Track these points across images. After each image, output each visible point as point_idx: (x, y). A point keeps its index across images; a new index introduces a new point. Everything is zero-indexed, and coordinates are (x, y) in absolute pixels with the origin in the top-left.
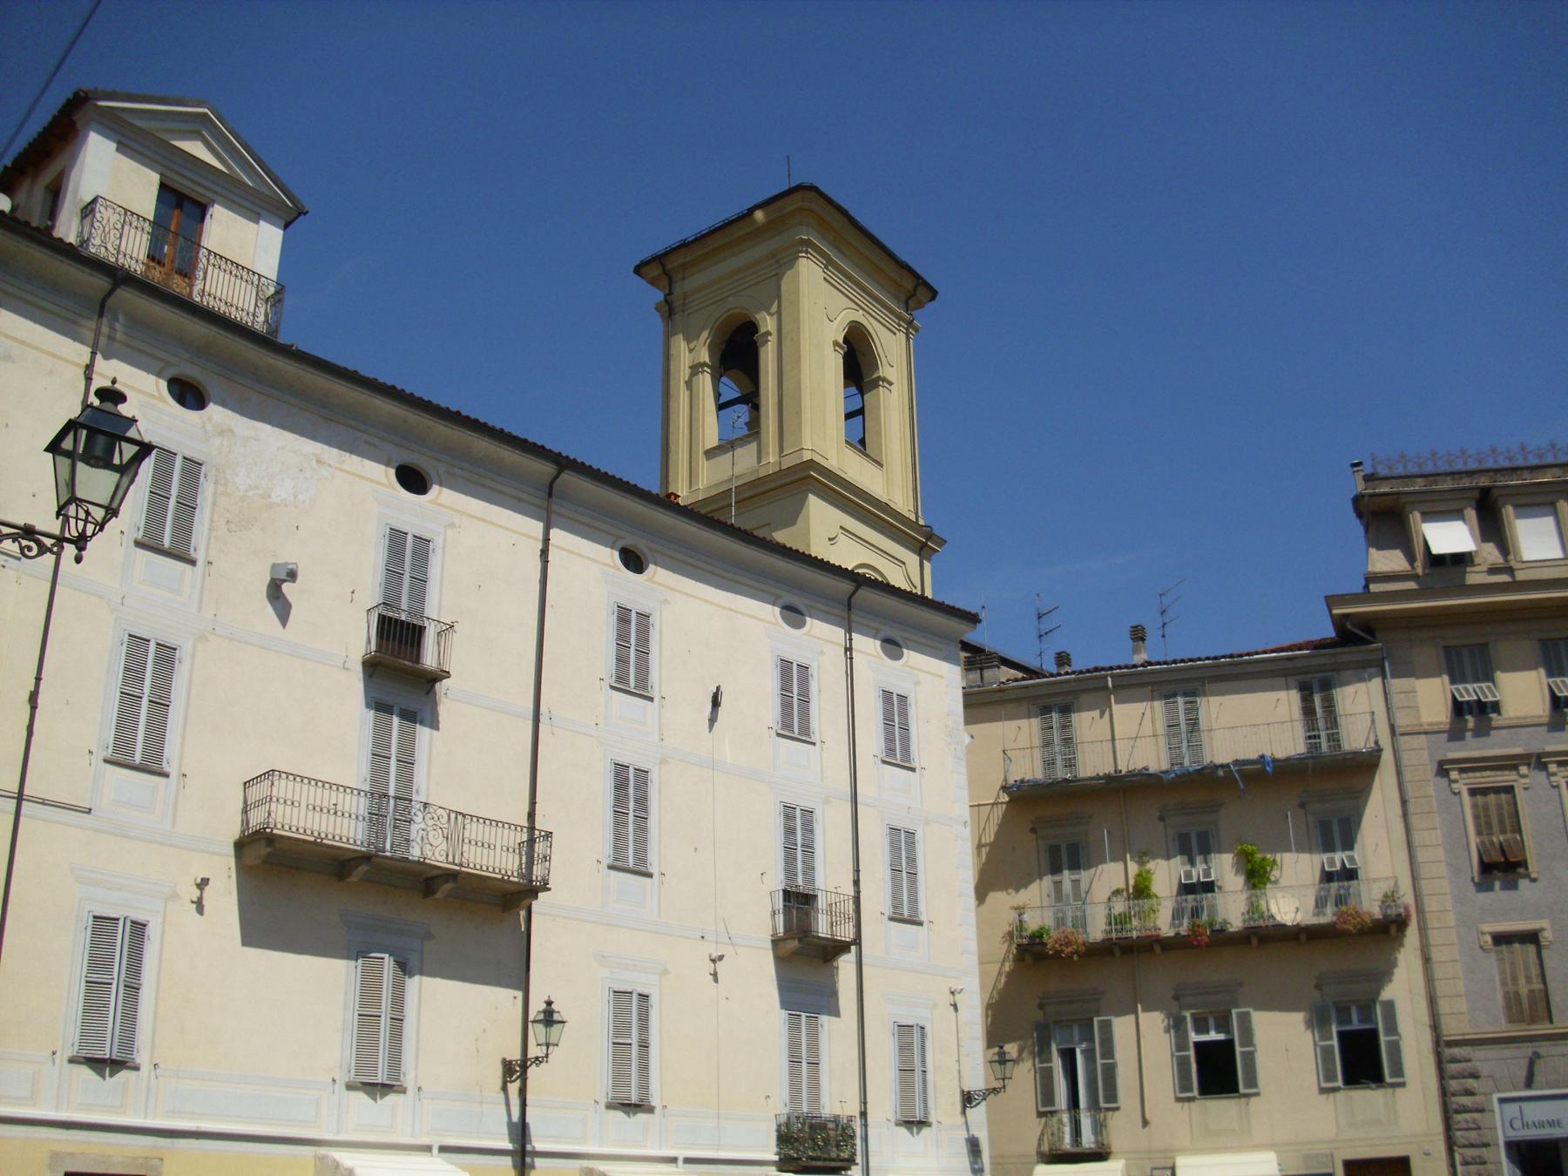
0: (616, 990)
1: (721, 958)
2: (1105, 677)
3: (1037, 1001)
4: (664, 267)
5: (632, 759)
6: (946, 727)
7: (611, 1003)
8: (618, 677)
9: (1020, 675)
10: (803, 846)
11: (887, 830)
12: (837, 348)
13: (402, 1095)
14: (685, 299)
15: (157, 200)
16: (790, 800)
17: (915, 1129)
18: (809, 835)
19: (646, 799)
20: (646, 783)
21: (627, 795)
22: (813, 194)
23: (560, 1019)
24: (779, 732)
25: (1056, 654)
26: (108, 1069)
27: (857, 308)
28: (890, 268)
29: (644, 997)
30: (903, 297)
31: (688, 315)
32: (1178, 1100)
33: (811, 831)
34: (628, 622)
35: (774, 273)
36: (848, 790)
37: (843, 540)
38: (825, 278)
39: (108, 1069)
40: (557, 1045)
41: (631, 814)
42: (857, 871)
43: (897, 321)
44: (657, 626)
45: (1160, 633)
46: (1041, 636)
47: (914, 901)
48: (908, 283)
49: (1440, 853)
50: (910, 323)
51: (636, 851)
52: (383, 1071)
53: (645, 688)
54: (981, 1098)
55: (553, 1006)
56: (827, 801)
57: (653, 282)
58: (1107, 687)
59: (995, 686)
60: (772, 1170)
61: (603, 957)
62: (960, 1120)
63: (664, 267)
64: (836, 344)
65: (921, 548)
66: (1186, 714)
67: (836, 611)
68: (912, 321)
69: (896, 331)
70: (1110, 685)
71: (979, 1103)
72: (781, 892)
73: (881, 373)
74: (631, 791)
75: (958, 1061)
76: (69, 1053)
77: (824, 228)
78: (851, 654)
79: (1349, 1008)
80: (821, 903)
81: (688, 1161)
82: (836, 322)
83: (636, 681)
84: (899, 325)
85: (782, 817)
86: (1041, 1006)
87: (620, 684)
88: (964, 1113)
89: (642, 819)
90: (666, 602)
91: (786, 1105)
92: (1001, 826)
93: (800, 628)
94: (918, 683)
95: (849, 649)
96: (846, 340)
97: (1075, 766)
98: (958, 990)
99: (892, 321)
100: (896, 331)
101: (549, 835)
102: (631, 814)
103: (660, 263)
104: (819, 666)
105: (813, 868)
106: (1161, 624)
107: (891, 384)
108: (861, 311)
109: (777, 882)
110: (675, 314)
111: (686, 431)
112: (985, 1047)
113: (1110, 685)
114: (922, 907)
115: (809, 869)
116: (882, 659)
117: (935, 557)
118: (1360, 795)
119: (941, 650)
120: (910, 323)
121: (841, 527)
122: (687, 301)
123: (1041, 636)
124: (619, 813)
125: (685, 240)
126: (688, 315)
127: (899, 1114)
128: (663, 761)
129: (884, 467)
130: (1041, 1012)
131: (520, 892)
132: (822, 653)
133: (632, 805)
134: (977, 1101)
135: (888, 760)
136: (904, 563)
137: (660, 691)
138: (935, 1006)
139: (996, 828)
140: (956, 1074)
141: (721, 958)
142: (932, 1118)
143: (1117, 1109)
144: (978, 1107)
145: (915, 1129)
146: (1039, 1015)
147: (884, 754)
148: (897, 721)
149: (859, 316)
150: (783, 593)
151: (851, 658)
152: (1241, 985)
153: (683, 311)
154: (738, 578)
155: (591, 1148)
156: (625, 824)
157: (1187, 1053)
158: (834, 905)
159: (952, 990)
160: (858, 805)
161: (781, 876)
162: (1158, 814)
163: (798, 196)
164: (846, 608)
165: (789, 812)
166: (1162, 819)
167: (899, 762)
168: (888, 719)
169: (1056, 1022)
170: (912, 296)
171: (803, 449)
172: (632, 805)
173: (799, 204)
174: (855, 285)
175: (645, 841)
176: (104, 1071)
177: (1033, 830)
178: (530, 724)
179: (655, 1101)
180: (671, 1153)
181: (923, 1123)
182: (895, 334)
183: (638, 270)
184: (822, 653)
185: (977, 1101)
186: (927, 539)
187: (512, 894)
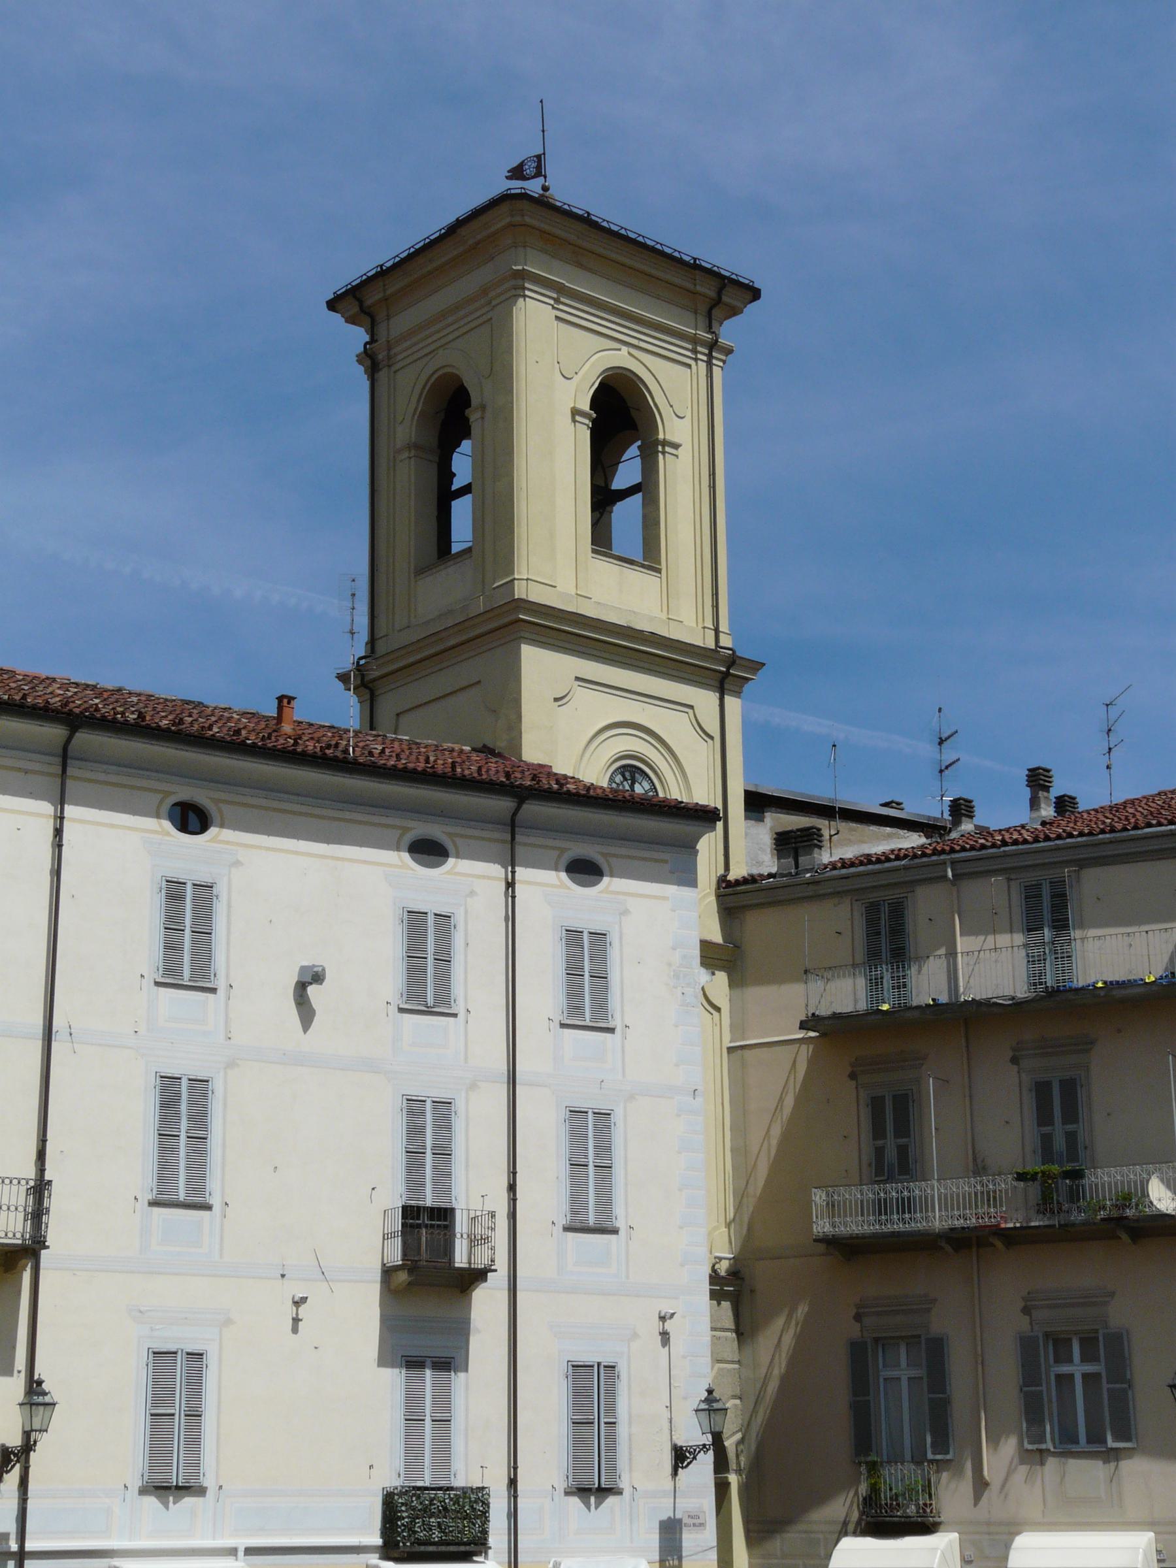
0: (155, 1350)
1: (304, 1300)
2: (944, 863)
4: (361, 302)
5: (185, 1066)
6: (670, 965)
7: (150, 1366)
8: (166, 970)
10: (434, 1147)
11: (564, 1114)
12: (578, 418)
13: (619, 1497)
14: (389, 350)
16: (415, 1091)
17: (593, 1499)
18: (444, 1133)
19: (205, 1115)
20: (205, 1096)
21: (178, 1114)
23: (51, 1401)
24: (401, 1006)
25: (1029, 770)
29: (196, 1356)
30: (703, 309)
31: (395, 372)
33: (449, 1128)
34: (182, 898)
35: (485, 318)
36: (503, 1067)
37: (583, 695)
38: (557, 318)
40: (46, 1431)
41: (183, 1135)
42: (513, 1173)
44: (224, 897)
45: (1104, 761)
46: (941, 771)
47: (605, 1202)
50: (713, 346)
51: (188, 1181)
52: (181, 1390)
53: (206, 977)
54: (692, 1456)
55: (44, 1385)
56: (473, 1086)
57: (351, 320)
58: (946, 876)
59: (808, 875)
60: (374, 1559)
61: (141, 1312)
62: (668, 1484)
63: (361, 302)
64: (575, 412)
66: (1053, 912)
67: (496, 835)
68: (717, 341)
70: (950, 874)
71: (691, 1462)
72: (400, 1209)
74: (184, 1107)
75: (670, 1408)
77: (554, 246)
78: (513, 892)
79: (1070, 1340)
80: (461, 1224)
81: (249, 1551)
82: (577, 379)
83: (193, 970)
85: (405, 1113)
86: (858, 1317)
87: (170, 979)
88: (675, 1473)
89: (199, 1140)
90: (238, 863)
91: (399, 1475)
94: (626, 912)
95: (510, 885)
96: (595, 402)
97: (905, 986)
98: (668, 1316)
99: (682, 350)
101: (50, 1182)
102: (183, 1135)
103: (355, 297)
104: (466, 912)
105: (449, 1175)
106: (1108, 750)
107: (676, 446)
108: (625, 349)
109: (393, 1196)
110: (379, 370)
111: (649, 345)
113: (950, 874)
114: (619, 1209)
115: (443, 1176)
116: (569, 888)
117: (748, 687)
119: (666, 862)
120: (713, 346)
121: (577, 679)
122: (392, 352)
123: (941, 771)
124: (166, 1137)
125: (381, 266)
126: (395, 372)
127: (570, 1479)
128: (231, 1064)
130: (857, 1326)
131: (16, 1251)
132: (472, 893)
133: (184, 1124)
134: (689, 1460)
135: (569, 1022)
136: (691, 707)
137: (227, 976)
138: (635, 1336)
140: (666, 1426)
141: (304, 1300)
142: (624, 1484)
144: (691, 1466)
145: (593, 1499)
146: (855, 1330)
147: (565, 1014)
148: (587, 968)
149: (622, 358)
150: (410, 824)
151: (513, 897)
153: (389, 366)
154: (347, 815)
155: (115, 1543)
156: (174, 1149)
158: (480, 1218)
159: (662, 1314)
160: (518, 1087)
161: (401, 1188)
162: (1011, 1054)
163: (504, 208)
165: (414, 1107)
166: (1015, 1060)
167: (588, 1023)
168: (573, 971)
169: (877, 1340)
170: (717, 302)
171: (515, 579)
172: (184, 1124)
173: (508, 220)
175: (203, 1166)
177: (853, 1076)
178: (38, 1046)
179: (208, 1481)
180: (229, 1542)
181: (604, 1492)
182: (689, 366)
183: (332, 305)
184: (472, 893)
185: (689, 1460)
187: (11, 1252)
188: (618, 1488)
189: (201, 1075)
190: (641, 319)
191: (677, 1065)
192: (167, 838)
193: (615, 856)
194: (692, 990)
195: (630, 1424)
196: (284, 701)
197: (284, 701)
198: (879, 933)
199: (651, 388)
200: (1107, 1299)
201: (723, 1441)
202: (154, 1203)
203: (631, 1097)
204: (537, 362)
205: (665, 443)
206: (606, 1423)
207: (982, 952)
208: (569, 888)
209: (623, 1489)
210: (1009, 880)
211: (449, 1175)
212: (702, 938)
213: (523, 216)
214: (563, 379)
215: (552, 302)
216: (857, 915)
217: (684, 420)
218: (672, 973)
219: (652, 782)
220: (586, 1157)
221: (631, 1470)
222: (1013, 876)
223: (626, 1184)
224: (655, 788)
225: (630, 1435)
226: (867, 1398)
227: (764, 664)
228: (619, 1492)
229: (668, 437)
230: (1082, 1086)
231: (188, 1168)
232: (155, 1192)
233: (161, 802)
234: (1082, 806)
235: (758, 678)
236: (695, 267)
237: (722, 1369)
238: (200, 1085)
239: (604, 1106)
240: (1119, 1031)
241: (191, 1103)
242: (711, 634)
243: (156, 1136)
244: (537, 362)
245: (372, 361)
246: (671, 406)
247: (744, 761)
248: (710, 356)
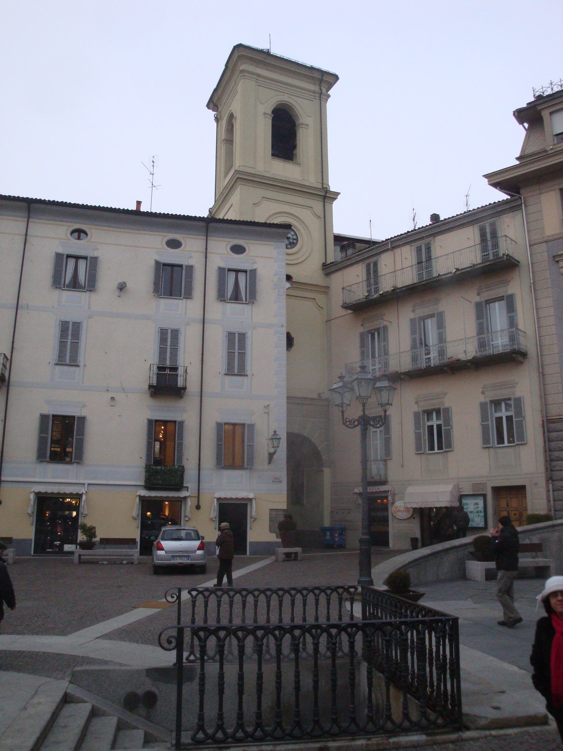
3: (481, 390)
5: (71, 318)
9: (367, 246)
15: (272, 147)
22: (241, 48)
27: (283, 94)
49: (552, 311)
56: (188, 324)
69: (313, 100)
73: (301, 122)
85: (159, 334)
86: (483, 393)
93: (180, 247)
100: (313, 100)
118: (230, 298)
128: (90, 317)
129: (302, 165)
149: (285, 98)
150: (167, 234)
152: (446, 394)
157: (488, 423)
164: (205, 234)
165: (163, 332)
172: (70, 337)
182: (313, 101)
189: (78, 321)
191: (275, 317)
192: (70, 241)
193: (250, 243)
196: (139, 203)
197: (139, 203)
198: (370, 273)
199: (294, 104)
202: (56, 364)
205: (302, 124)
207: (399, 273)
210: (411, 246)
211: (176, 355)
212: (288, 274)
215: (255, 80)
216: (363, 268)
220: (234, 349)
222: (412, 244)
223: (86, 343)
226: (488, 423)
227: (340, 193)
229: (304, 122)
231: (70, 352)
232: (57, 361)
233: (68, 229)
234: (442, 218)
235: (339, 197)
236: (312, 69)
238: (77, 326)
239: (242, 331)
241: (73, 330)
242: (321, 185)
245: (217, 119)
248: (320, 97)
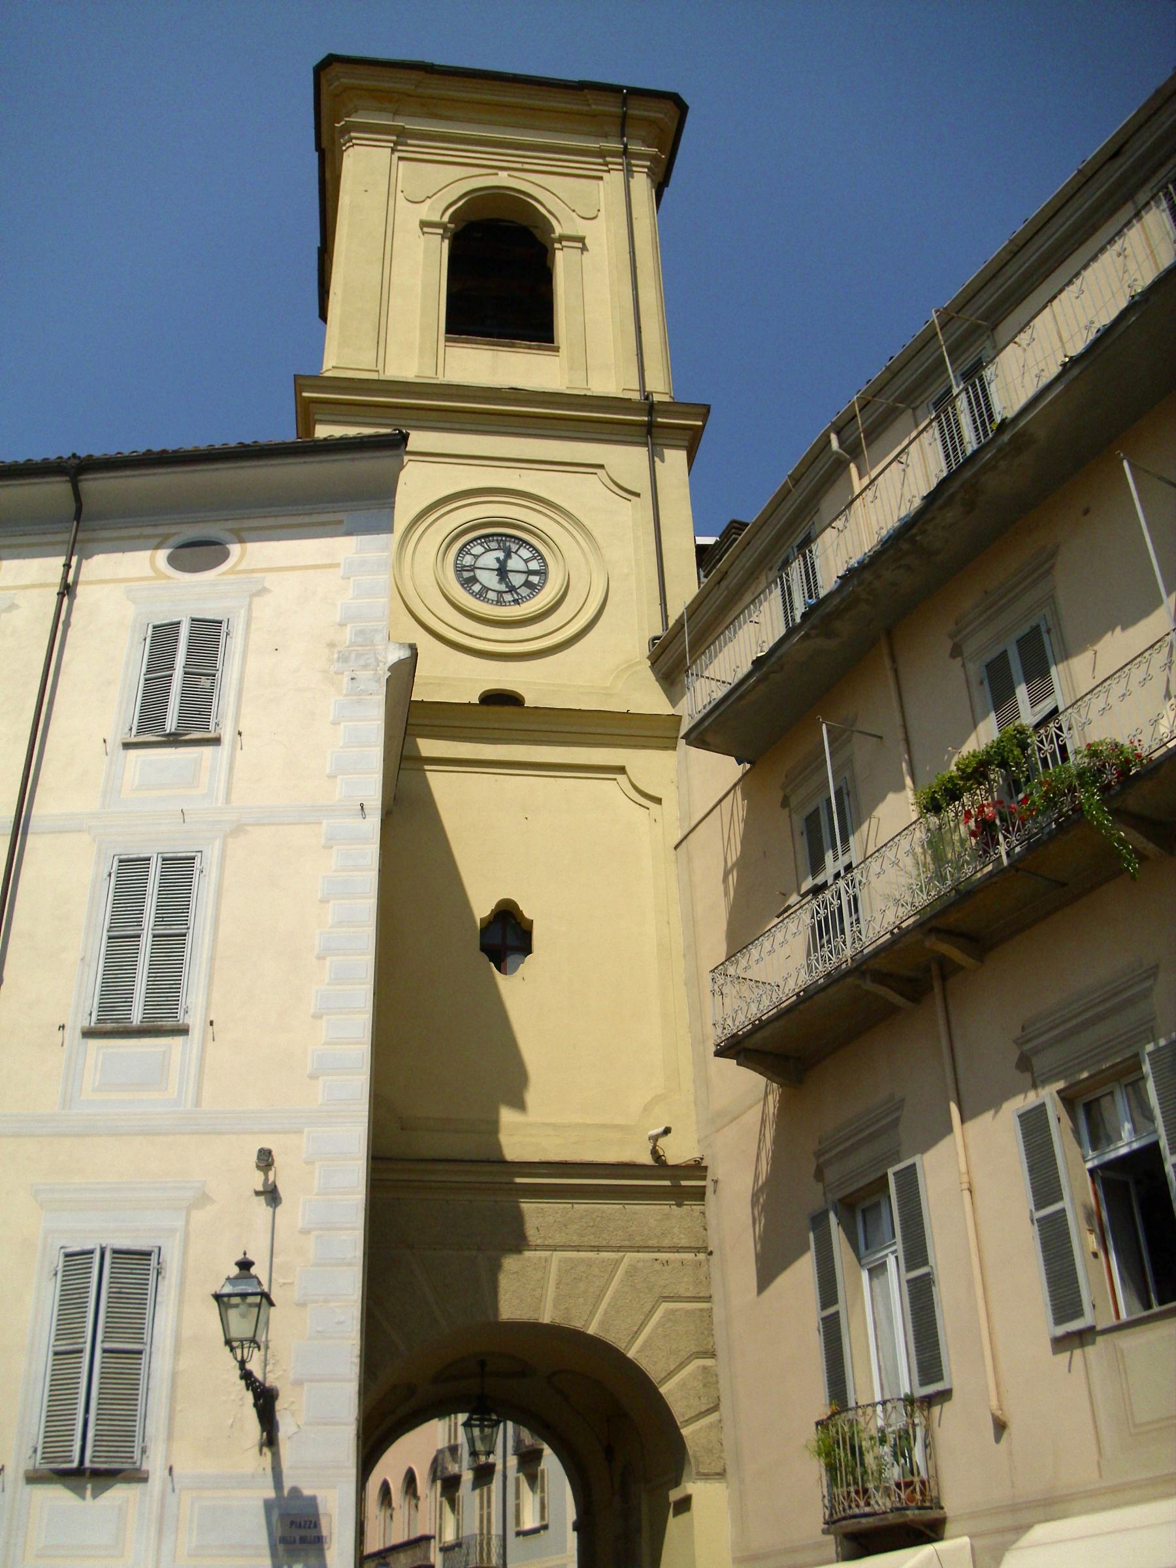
6: (332, 645)
12: (425, 230)
13: (141, 1486)
22: (337, 68)
26: (89, 1486)
28: (561, 102)
32: (1061, 1344)
39: (89, 1486)
43: (601, 161)
48: (611, 107)
65: (649, 433)
76: (26, 1465)
84: (606, 164)
92: (746, 822)
99: (592, 165)
108: (500, 173)
112: (819, 1308)
119: (340, 522)
136: (601, 467)
139: (742, 826)
142: (154, 1464)
143: (946, 1395)
174: (443, 141)
176: (85, 1489)
182: (601, 178)
186: (650, 414)
188: (138, 1470)
190: (519, 144)
194: (373, 672)
195: (177, 1352)
200: (1147, 984)
201: (677, 1429)
203: (239, 829)
204: (366, 191)
206: (105, 1351)
208: (169, 578)
209: (148, 1472)
213: (339, 80)
214: (410, 204)
217: (598, 218)
218: (336, 656)
219: (531, 546)
221: (170, 1437)
224: (540, 554)
225: (174, 1375)
228: (143, 1479)
230: (1048, 631)
237: (673, 1311)
240: (1086, 512)
243: (717, 1292)
244: (366, 191)
246: (574, 211)
247: (693, 517)
